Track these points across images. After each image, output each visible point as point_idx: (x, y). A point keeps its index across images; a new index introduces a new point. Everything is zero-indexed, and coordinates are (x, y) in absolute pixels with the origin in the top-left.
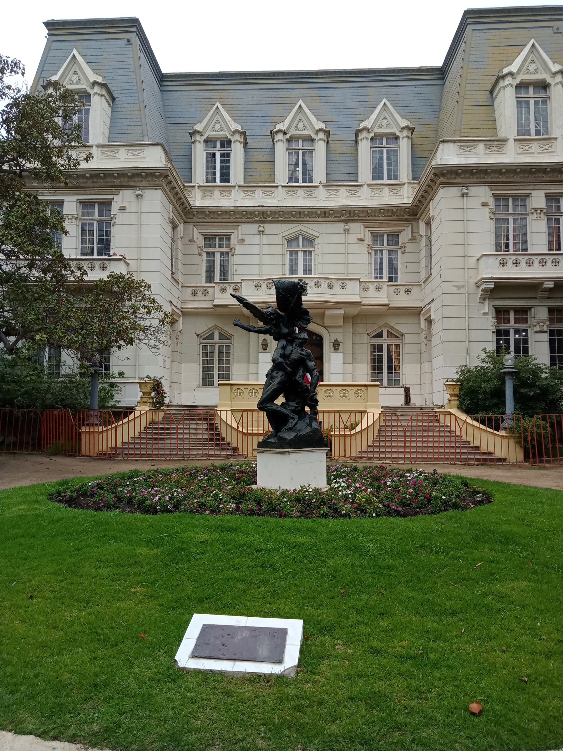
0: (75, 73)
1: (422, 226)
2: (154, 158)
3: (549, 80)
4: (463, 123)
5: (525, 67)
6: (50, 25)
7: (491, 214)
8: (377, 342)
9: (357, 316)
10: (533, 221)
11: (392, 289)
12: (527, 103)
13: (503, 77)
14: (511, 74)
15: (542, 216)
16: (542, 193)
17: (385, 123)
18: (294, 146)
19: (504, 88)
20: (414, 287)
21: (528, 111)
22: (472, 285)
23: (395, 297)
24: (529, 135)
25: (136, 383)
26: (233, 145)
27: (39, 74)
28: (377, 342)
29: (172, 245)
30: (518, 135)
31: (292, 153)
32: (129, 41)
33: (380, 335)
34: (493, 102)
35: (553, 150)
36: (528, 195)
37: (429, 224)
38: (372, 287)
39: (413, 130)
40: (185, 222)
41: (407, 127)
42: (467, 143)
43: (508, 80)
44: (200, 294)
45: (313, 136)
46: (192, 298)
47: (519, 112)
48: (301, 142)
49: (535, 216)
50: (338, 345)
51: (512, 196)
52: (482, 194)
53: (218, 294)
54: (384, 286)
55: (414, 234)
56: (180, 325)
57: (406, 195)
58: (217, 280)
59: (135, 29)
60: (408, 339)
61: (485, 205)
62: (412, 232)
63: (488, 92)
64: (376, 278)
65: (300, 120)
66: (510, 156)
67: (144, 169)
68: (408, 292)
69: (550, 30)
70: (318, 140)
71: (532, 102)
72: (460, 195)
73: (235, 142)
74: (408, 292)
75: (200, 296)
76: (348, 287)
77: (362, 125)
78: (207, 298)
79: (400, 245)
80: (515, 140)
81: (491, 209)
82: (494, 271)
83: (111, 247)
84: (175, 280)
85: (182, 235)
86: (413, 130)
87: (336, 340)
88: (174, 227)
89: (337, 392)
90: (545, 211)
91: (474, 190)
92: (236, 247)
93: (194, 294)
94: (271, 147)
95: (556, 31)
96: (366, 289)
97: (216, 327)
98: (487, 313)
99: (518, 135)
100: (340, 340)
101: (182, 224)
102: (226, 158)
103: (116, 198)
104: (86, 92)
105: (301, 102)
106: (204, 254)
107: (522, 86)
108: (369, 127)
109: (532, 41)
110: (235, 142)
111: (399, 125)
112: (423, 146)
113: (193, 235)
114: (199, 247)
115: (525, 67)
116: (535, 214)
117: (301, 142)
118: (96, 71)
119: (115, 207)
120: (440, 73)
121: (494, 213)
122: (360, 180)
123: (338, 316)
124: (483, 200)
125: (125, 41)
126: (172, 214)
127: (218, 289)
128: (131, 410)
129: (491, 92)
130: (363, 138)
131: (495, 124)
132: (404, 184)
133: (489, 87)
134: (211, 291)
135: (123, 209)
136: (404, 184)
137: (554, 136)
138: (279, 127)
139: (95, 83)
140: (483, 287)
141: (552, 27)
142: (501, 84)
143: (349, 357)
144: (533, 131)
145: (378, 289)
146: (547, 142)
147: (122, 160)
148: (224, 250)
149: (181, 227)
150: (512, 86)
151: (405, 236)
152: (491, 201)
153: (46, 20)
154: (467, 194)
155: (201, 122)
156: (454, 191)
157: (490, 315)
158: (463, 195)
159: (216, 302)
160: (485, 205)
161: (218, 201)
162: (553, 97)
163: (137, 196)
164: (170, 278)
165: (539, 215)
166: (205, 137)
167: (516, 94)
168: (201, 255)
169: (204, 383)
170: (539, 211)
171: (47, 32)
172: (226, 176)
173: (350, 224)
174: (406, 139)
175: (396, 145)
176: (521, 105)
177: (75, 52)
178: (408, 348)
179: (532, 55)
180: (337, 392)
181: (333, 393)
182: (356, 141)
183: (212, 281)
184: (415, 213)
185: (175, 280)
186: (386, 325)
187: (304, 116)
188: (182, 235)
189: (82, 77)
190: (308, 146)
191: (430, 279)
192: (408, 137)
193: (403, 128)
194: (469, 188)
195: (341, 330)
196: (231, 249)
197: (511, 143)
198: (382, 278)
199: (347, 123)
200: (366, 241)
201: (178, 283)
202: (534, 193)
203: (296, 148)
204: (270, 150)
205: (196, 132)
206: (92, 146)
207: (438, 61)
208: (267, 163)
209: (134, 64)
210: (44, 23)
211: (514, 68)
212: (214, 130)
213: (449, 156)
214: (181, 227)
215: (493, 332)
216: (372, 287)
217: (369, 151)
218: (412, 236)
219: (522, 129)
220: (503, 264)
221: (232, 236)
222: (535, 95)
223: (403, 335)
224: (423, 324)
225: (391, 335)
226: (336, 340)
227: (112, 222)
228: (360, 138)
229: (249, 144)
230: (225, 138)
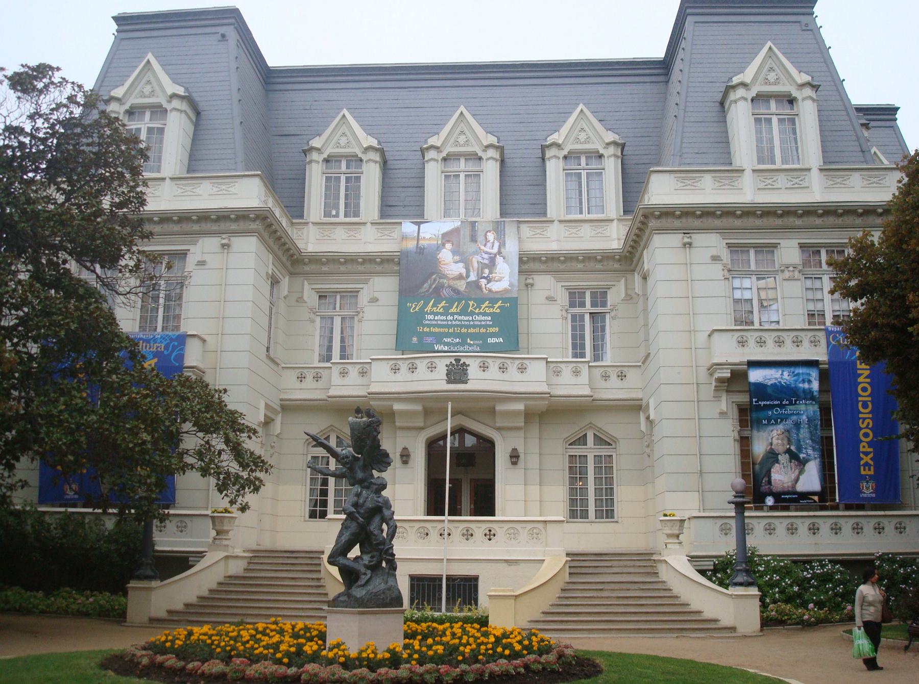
0: (149, 82)
1: (637, 278)
2: (249, 194)
3: (795, 93)
4: (684, 145)
5: (762, 76)
6: (116, 19)
7: (726, 271)
8: (577, 451)
9: (545, 413)
10: (785, 283)
11: (597, 373)
12: (769, 121)
13: (733, 87)
14: (743, 85)
15: (796, 274)
16: (795, 243)
17: (583, 136)
18: (453, 167)
19: (735, 102)
20: (631, 370)
21: (770, 131)
22: (703, 372)
23: (604, 384)
24: (774, 163)
25: (207, 515)
26: (365, 167)
27: (99, 82)
28: (577, 451)
29: (271, 309)
30: (759, 163)
31: (573, 176)
32: (223, 36)
33: (582, 440)
34: (725, 117)
35: (806, 185)
36: (775, 246)
37: (645, 278)
38: (567, 371)
39: (623, 146)
40: (292, 274)
41: (615, 143)
42: (687, 174)
43: (741, 92)
44: (309, 378)
45: (480, 154)
46: (298, 385)
47: (759, 132)
48: (462, 161)
49: (787, 275)
50: (518, 457)
51: (754, 247)
52: (710, 243)
53: (336, 378)
54: (585, 369)
55: (629, 292)
56: (277, 427)
57: (615, 236)
58: (336, 358)
59: (233, 21)
60: (623, 447)
61: (716, 258)
62: (626, 289)
63: (718, 104)
64: (575, 355)
65: (462, 132)
66: (747, 192)
67: (233, 210)
68: (622, 376)
69: (796, 27)
70: (488, 159)
71: (775, 119)
72: (680, 245)
73: (367, 161)
74: (622, 376)
75: (309, 382)
76: (529, 370)
77: (550, 140)
78: (320, 384)
79: (609, 307)
80: (754, 171)
81: (725, 266)
82: (729, 352)
83: (183, 317)
84: (273, 361)
85: (286, 293)
86: (623, 146)
87: (515, 450)
88: (274, 282)
89: (524, 533)
90: (800, 268)
91: (699, 239)
92: (365, 309)
93: (301, 378)
94: (420, 166)
95: (804, 28)
96: (558, 373)
97: (332, 428)
98: (726, 413)
99: (759, 163)
100: (521, 450)
101: (287, 278)
102: (354, 182)
103: (192, 248)
104: (161, 106)
105: (462, 108)
106: (318, 319)
107: (760, 99)
108: (560, 142)
109: (769, 44)
110: (367, 161)
111: (603, 141)
112: (639, 166)
113: (302, 292)
114: (312, 311)
115: (762, 76)
116: (786, 272)
117: (462, 161)
118: (175, 81)
119: (191, 260)
120: (662, 69)
121: (729, 271)
122: (549, 215)
123: (515, 413)
124: (714, 252)
125: (219, 37)
126: (271, 266)
127: (335, 371)
128: (200, 555)
129: (722, 104)
130: (552, 157)
131: (729, 147)
132: (612, 220)
133: (719, 97)
134: (325, 373)
135: (201, 263)
136: (612, 220)
137: (806, 166)
138: (433, 141)
139: (174, 96)
140: (717, 375)
141: (799, 22)
142: (732, 96)
143: (534, 475)
144: (778, 159)
145: (576, 373)
146: (799, 173)
147: (206, 197)
148: (346, 313)
149: (285, 282)
150: (746, 99)
151: (615, 295)
152: (725, 255)
153: (115, 14)
154: (690, 244)
155: (320, 135)
156: (676, 239)
157: (730, 413)
158: (685, 245)
159: (333, 392)
160: (716, 258)
161: (340, 242)
162: (801, 115)
163: (223, 245)
164: (264, 357)
165: (791, 274)
166: (325, 155)
167: (753, 109)
168: (313, 321)
169: (313, 515)
170: (791, 269)
171: (116, 27)
172: (353, 208)
173: (535, 277)
174: (612, 159)
175: (599, 167)
176: (761, 124)
177: (150, 56)
178: (622, 463)
179: (770, 61)
180: (524, 533)
181: (407, 533)
182: (543, 159)
183: (328, 358)
184: (629, 259)
185: (273, 361)
186: (591, 426)
187: (465, 127)
188: (286, 293)
189: (157, 88)
190: (472, 167)
191: (650, 358)
192: (616, 156)
193: (608, 144)
194: (693, 235)
195: (522, 433)
196: (358, 312)
197: (748, 174)
198: (583, 355)
199: (531, 133)
200: (559, 301)
201: (278, 364)
202: (783, 243)
203: (456, 169)
204: (419, 171)
205: (312, 149)
206: (165, 179)
207: (659, 53)
208: (414, 189)
209: (231, 109)
210: (113, 18)
211: (747, 76)
212: (338, 145)
213: (662, 191)
214: (285, 282)
215: (735, 440)
216: (567, 371)
217: (562, 175)
218: (627, 294)
219: (764, 154)
220: (742, 343)
221: (360, 295)
222: (778, 112)
223: (616, 440)
224: (643, 426)
225: (599, 441)
226: (515, 450)
227: (187, 283)
228: (547, 156)
229: (389, 162)
230: (353, 156)
